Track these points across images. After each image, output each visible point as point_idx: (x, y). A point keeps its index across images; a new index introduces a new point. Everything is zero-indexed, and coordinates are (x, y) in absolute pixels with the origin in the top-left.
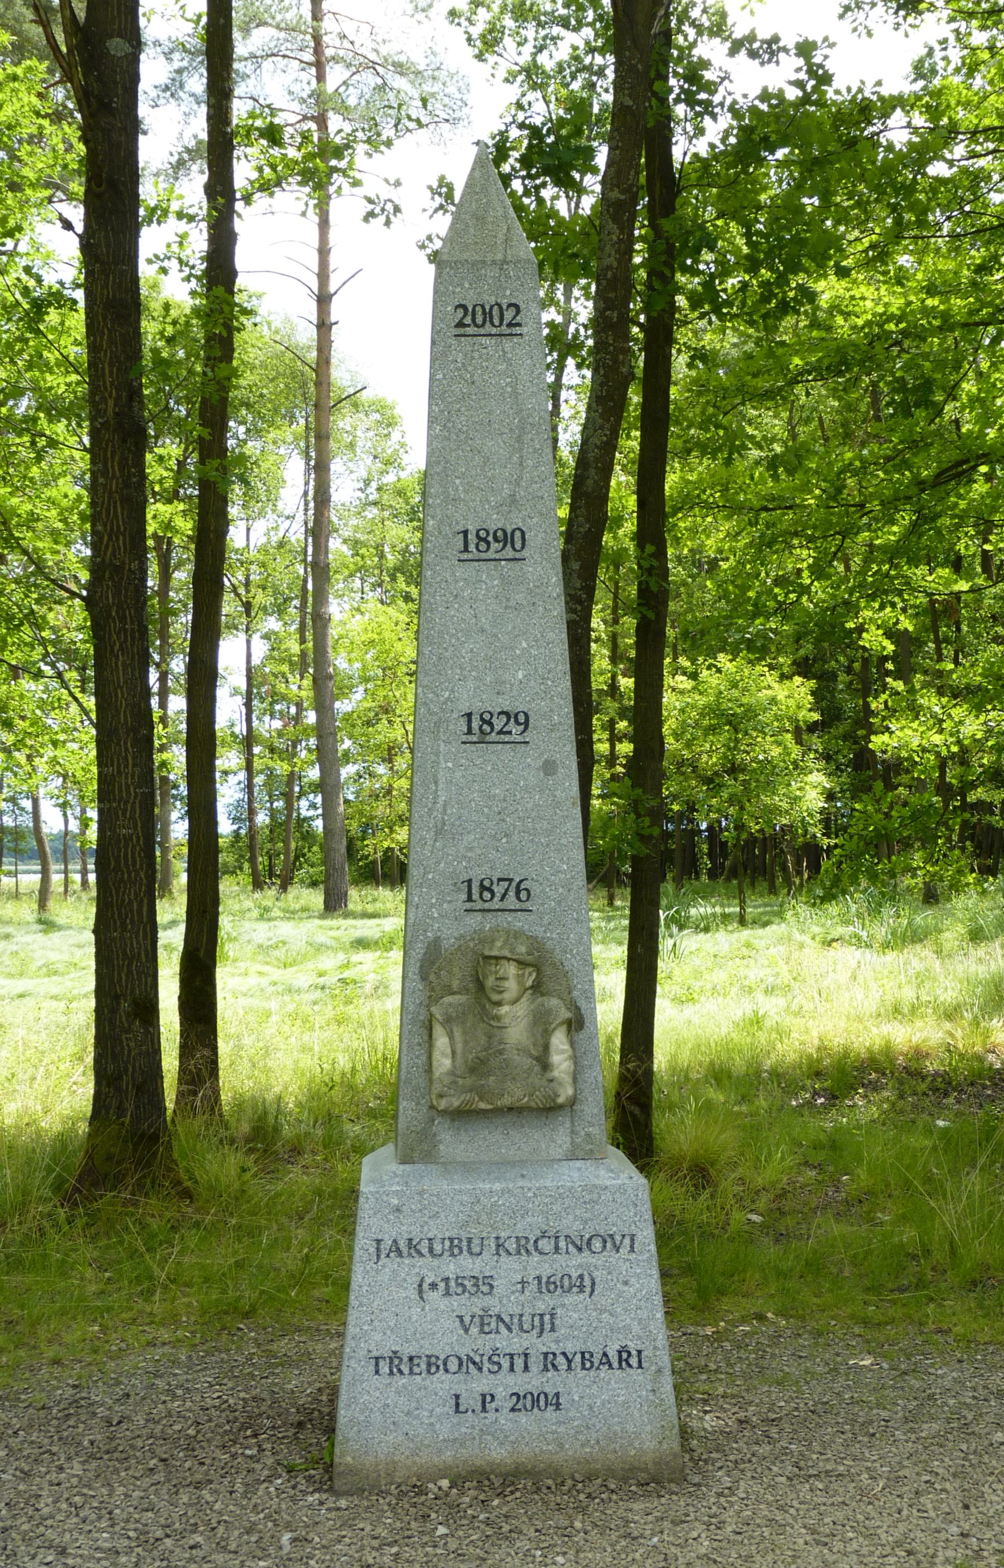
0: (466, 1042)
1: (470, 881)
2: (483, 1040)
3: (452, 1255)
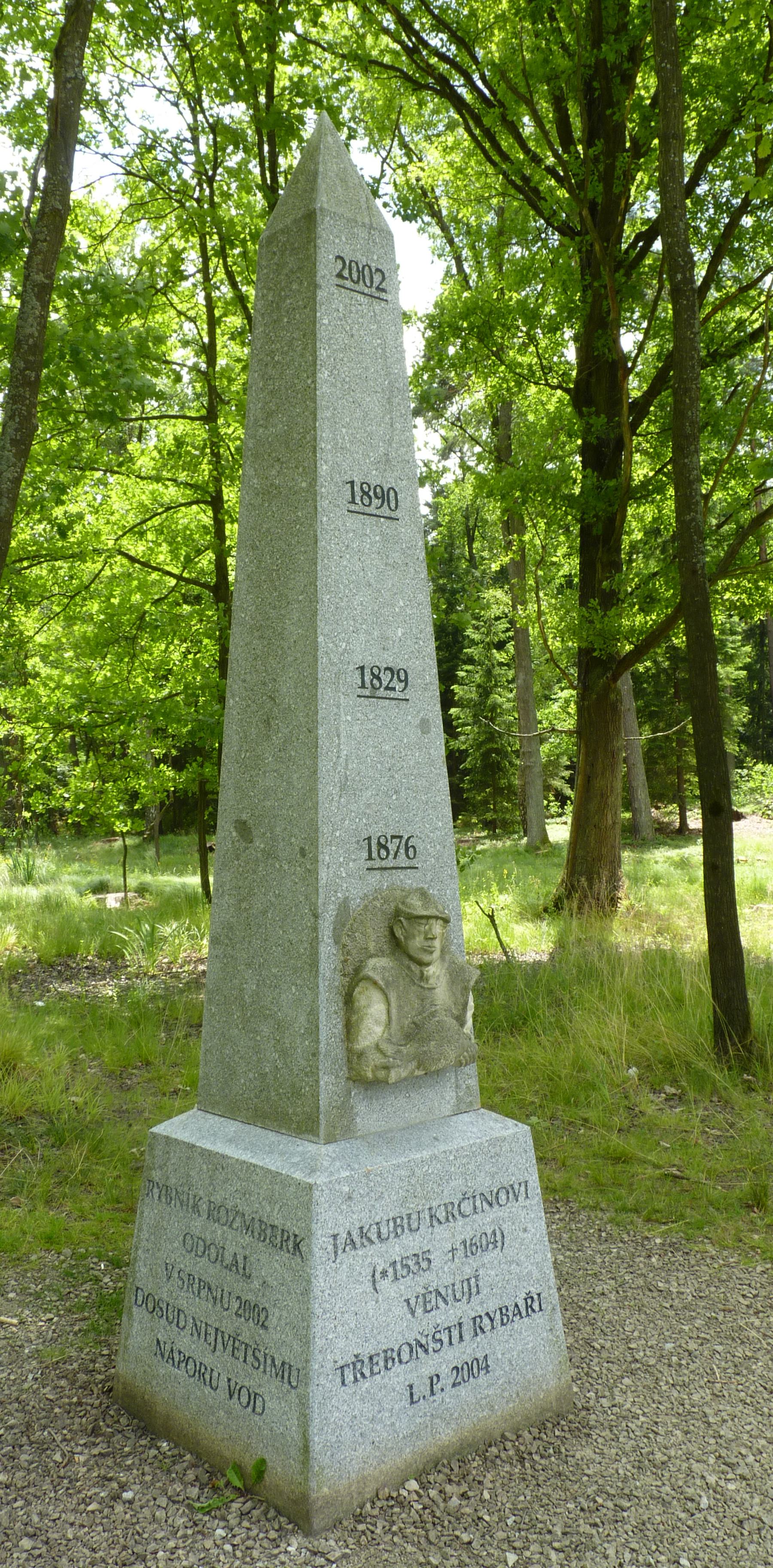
0: (400, 1007)
1: (369, 838)
2: (416, 1003)
3: (397, 1235)
